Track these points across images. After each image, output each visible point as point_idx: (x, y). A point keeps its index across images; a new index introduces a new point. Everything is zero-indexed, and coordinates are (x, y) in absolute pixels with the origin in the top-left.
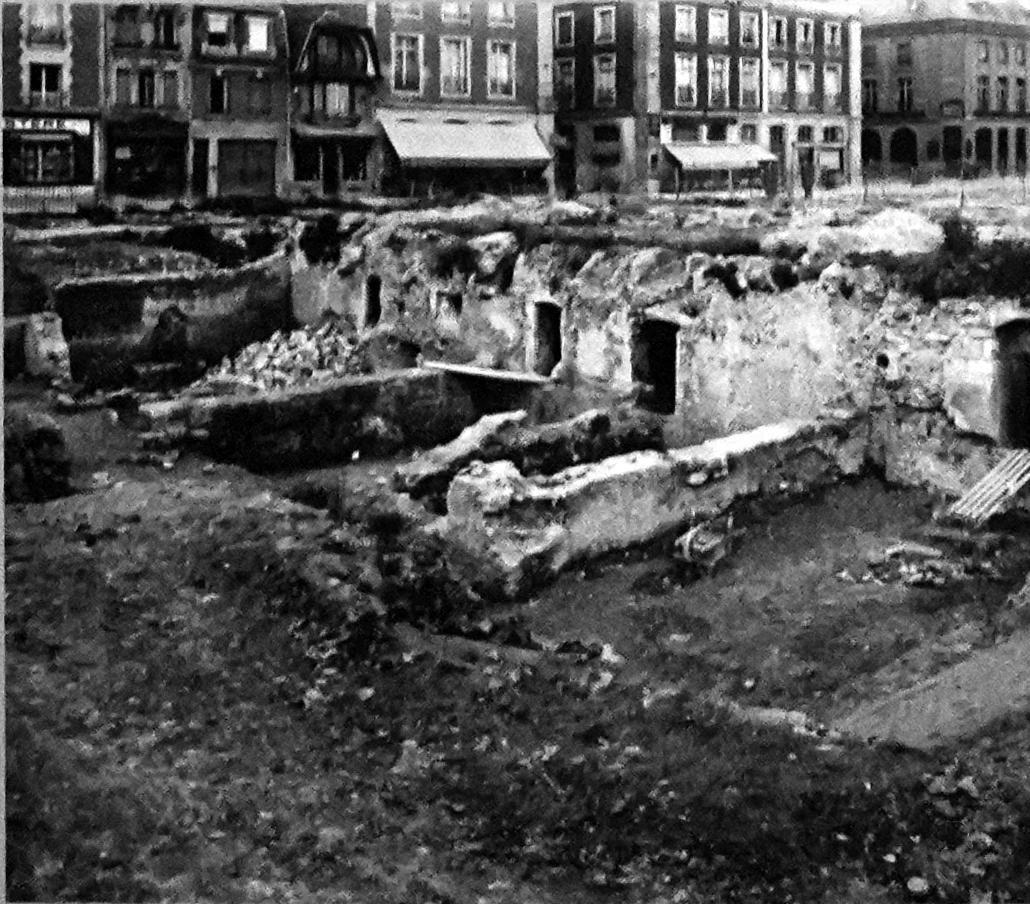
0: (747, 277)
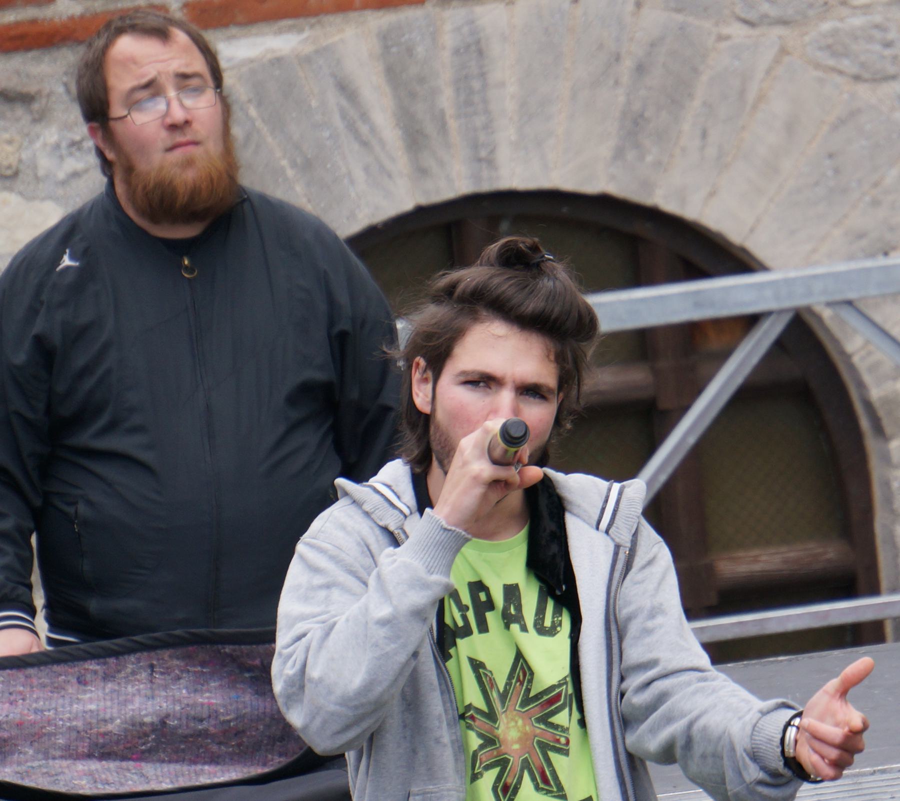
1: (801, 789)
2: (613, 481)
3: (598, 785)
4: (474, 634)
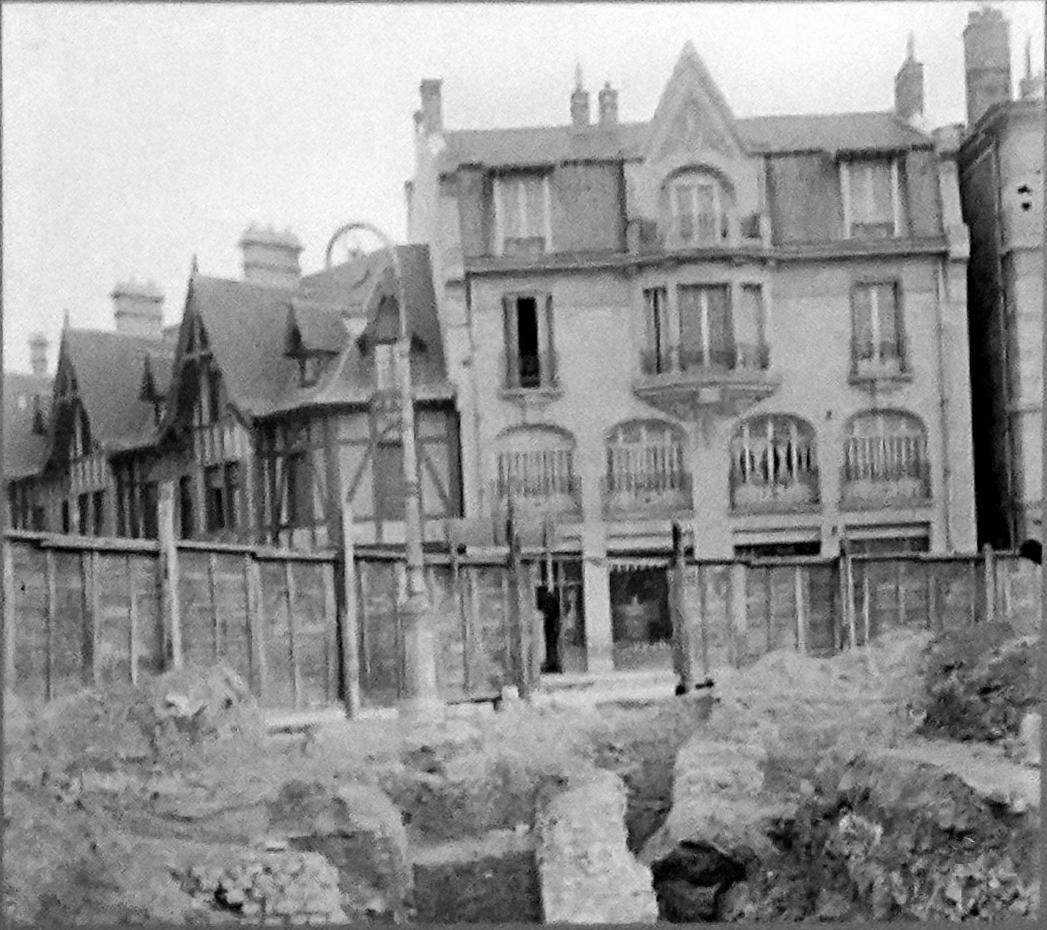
0: (765, 435)
4: (1019, 81)
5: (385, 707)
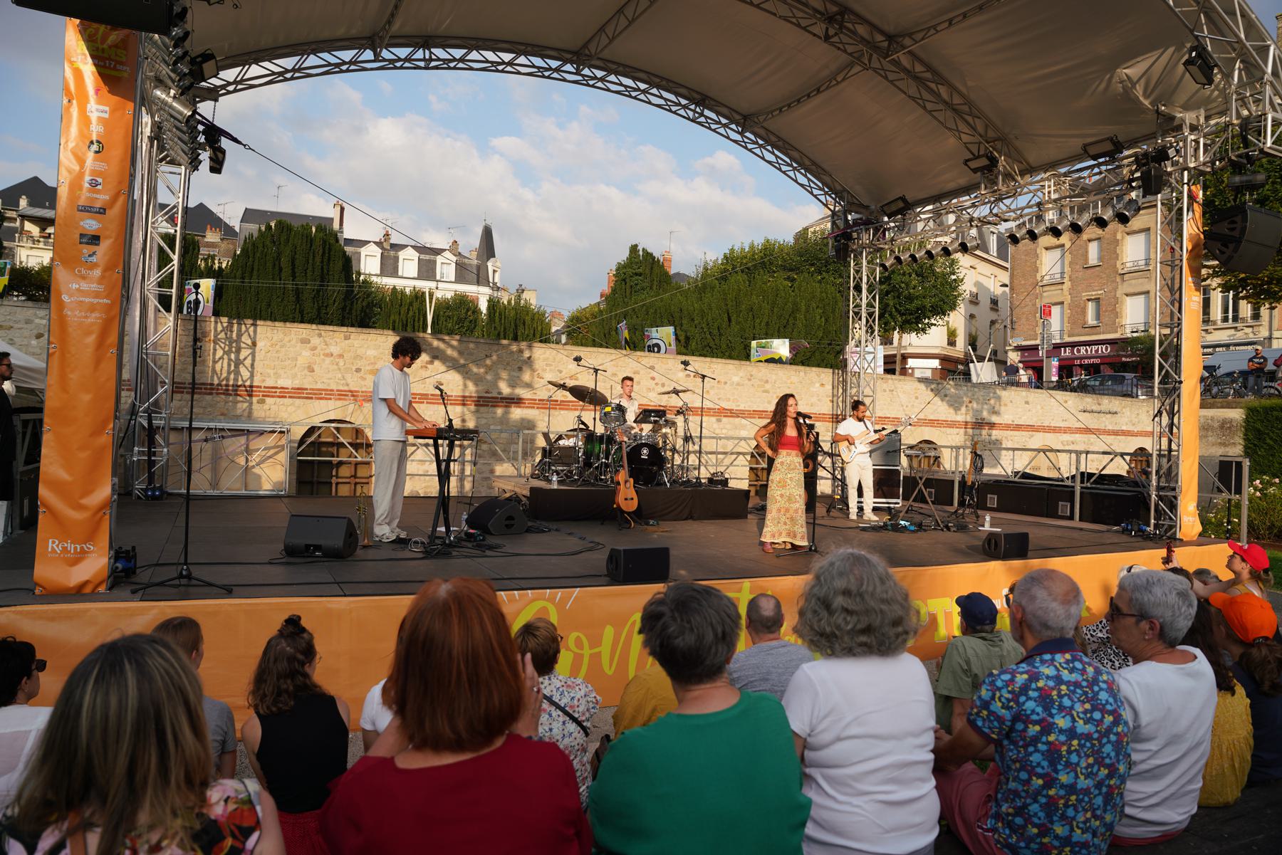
1: (377, 517)
2: (25, 678)
3: (396, 417)
5: (620, 268)
